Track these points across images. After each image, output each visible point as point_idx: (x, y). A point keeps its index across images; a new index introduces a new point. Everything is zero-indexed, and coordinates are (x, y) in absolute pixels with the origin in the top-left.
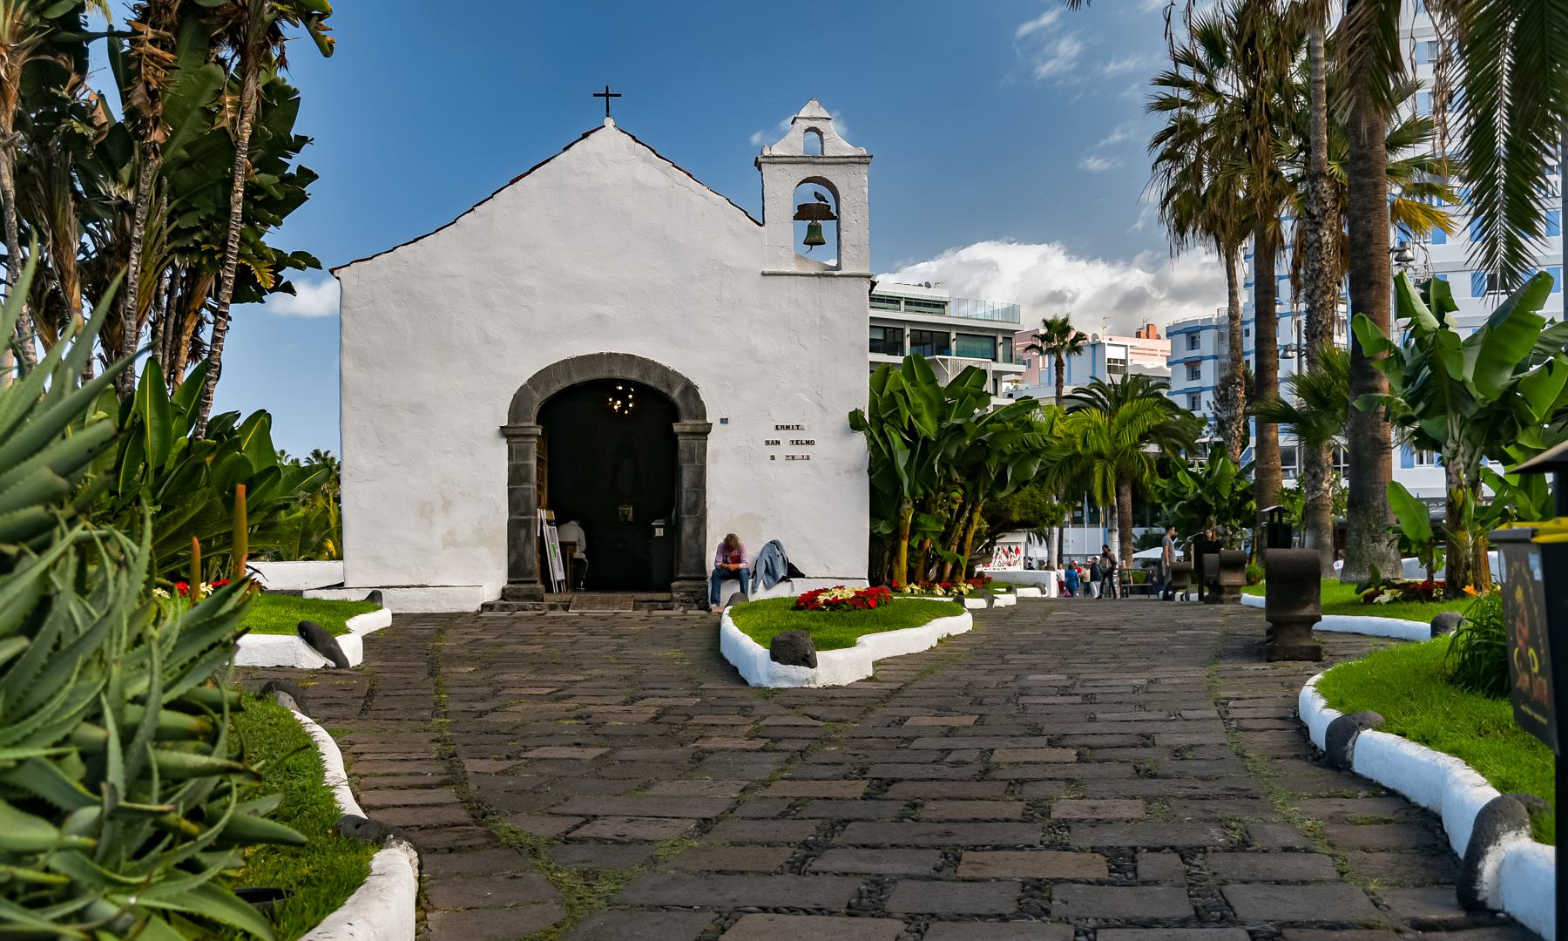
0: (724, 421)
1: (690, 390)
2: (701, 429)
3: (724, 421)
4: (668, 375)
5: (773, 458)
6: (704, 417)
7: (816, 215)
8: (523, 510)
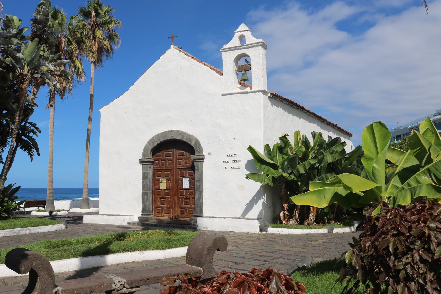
0: (209, 154)
1: (197, 142)
2: (200, 157)
3: (209, 154)
5: (226, 168)
6: (202, 152)
7: (244, 68)
8: (146, 189)
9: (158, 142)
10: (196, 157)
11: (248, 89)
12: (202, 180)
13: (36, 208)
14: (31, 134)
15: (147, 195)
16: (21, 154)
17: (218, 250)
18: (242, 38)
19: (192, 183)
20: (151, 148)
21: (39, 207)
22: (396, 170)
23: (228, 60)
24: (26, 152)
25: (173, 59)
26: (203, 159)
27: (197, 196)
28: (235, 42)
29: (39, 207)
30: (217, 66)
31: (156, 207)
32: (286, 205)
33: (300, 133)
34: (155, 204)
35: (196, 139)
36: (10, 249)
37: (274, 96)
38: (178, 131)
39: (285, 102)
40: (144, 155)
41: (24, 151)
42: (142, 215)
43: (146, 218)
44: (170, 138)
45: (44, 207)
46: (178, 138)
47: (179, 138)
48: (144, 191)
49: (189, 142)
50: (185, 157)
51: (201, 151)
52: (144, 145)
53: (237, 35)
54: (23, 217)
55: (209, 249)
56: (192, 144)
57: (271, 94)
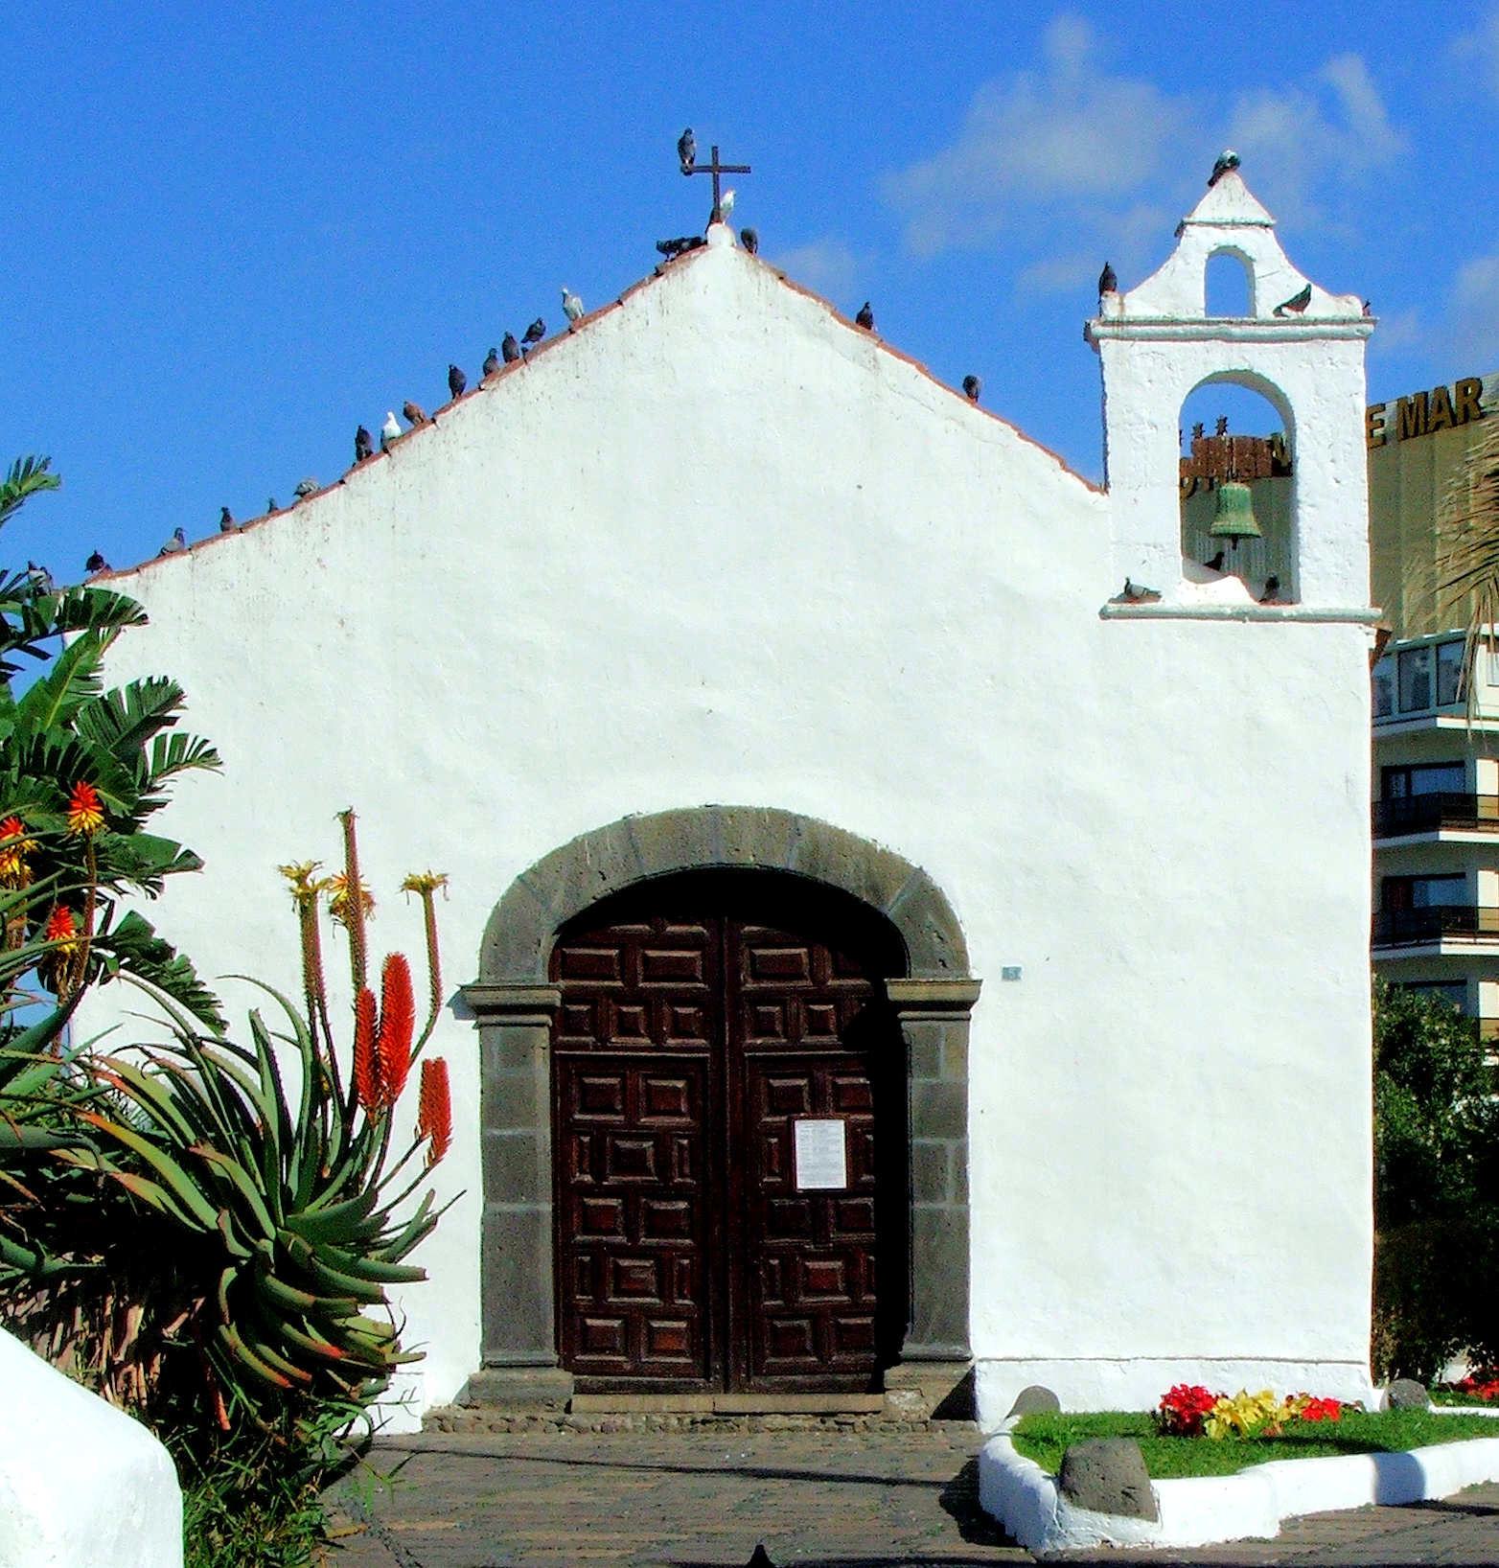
0: (1011, 974)
1: (928, 899)
2: (953, 993)
3: (1011, 974)
4: (881, 864)
6: (961, 960)
7: (1235, 484)
9: (617, 881)
10: (921, 993)
11: (1286, 610)
18: (1230, 274)
20: (562, 906)
22: (859, 1244)
23: (1149, 398)
25: (727, 339)
26: (965, 1005)
28: (1178, 286)
30: (1074, 432)
32: (802, 1298)
38: (783, 824)
42: (486, 1365)
44: (708, 860)
46: (778, 863)
47: (786, 859)
48: (1385, 731)
50: (806, 983)
53: (1198, 243)
54: (1344, 322)
56: (892, 910)
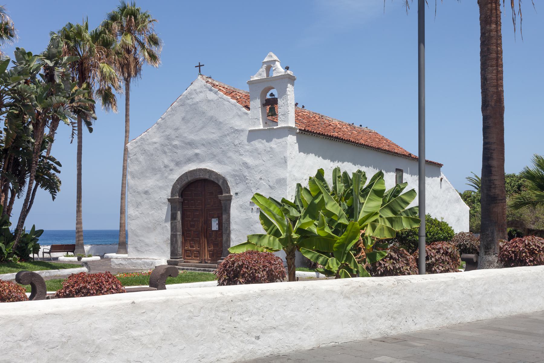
0: (237, 194)
1: (225, 181)
6: (230, 193)
12: (230, 221)
13: (65, 253)
14: (52, 171)
15: (176, 238)
16: (42, 193)
17: (170, 276)
19: (220, 224)
21: (67, 252)
24: (48, 190)
27: (224, 239)
29: (67, 252)
31: (186, 251)
33: (340, 170)
34: (184, 247)
35: (224, 178)
36: (176, 176)
37: (303, 132)
39: (321, 136)
40: (173, 194)
41: (45, 189)
43: (175, 261)
45: (73, 252)
47: (207, 177)
49: (216, 182)
51: (229, 192)
52: (172, 184)
55: (162, 275)
56: (220, 183)
57: (300, 130)
